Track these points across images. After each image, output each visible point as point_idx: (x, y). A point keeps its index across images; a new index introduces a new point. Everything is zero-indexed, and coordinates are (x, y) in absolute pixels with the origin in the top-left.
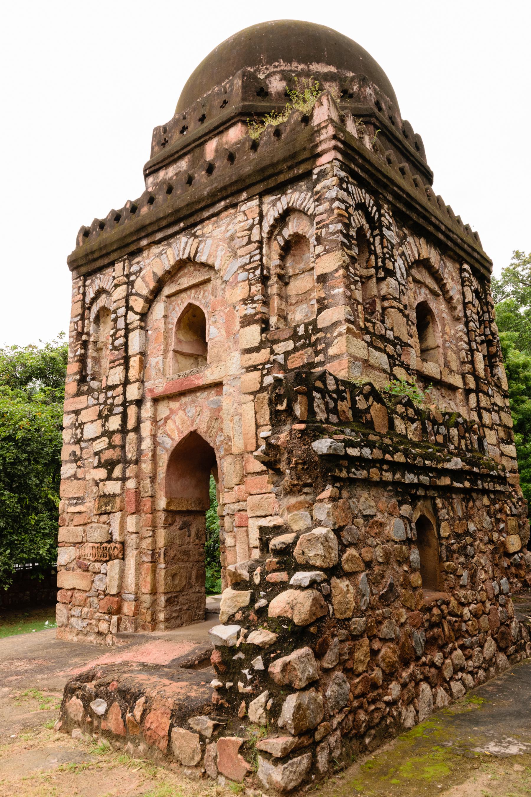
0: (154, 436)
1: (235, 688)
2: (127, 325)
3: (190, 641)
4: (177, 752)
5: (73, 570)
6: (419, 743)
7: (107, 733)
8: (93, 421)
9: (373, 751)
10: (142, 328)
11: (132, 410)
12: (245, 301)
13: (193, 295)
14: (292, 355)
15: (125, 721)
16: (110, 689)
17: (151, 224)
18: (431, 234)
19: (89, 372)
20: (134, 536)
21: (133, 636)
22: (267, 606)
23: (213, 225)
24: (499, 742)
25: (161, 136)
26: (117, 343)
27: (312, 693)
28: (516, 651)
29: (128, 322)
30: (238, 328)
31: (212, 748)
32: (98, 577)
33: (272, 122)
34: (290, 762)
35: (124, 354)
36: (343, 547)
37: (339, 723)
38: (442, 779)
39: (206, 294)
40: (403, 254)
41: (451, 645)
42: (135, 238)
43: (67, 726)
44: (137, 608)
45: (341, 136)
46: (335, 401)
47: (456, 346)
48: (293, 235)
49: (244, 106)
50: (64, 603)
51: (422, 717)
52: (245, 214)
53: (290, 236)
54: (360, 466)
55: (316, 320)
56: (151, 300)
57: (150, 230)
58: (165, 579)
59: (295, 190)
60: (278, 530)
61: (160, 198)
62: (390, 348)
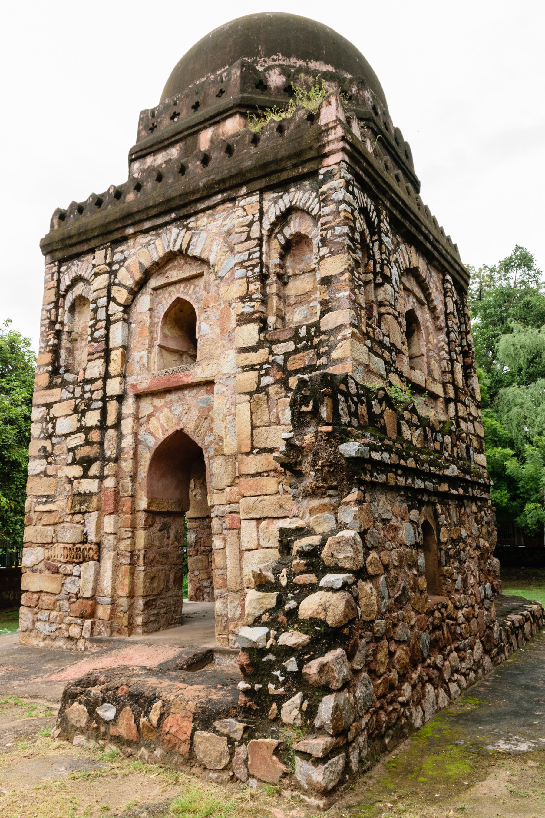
0: (136, 434)
1: (264, 691)
2: (108, 316)
3: (173, 645)
4: (200, 756)
5: (41, 572)
6: (432, 742)
7: (117, 740)
8: (67, 416)
9: (391, 751)
10: (125, 320)
11: (112, 406)
12: (242, 299)
13: (182, 289)
14: (293, 357)
15: (138, 726)
16: (119, 693)
17: (138, 212)
18: (421, 243)
19: (62, 363)
20: (112, 537)
21: (109, 641)
22: (297, 607)
23: (208, 218)
24: (507, 740)
25: (149, 121)
26: (97, 335)
27: (345, 694)
28: (498, 654)
29: (109, 313)
30: (234, 326)
31: (242, 751)
32: (69, 579)
33: (273, 118)
34: (329, 762)
35: (104, 347)
36: (367, 550)
37: (367, 724)
38: (466, 776)
39: (197, 289)
40: (396, 261)
41: (449, 648)
42: (119, 225)
43: (67, 731)
44: (113, 611)
45: (349, 138)
46: (356, 404)
47: (439, 355)
48: (294, 235)
49: (243, 98)
50: (29, 607)
51: (428, 717)
52: (244, 210)
53: (291, 235)
54: (380, 470)
55: (319, 322)
56: (136, 291)
57: (137, 218)
58: (144, 582)
59: (299, 189)
60: (300, 532)
61: (148, 185)
62: (386, 354)
